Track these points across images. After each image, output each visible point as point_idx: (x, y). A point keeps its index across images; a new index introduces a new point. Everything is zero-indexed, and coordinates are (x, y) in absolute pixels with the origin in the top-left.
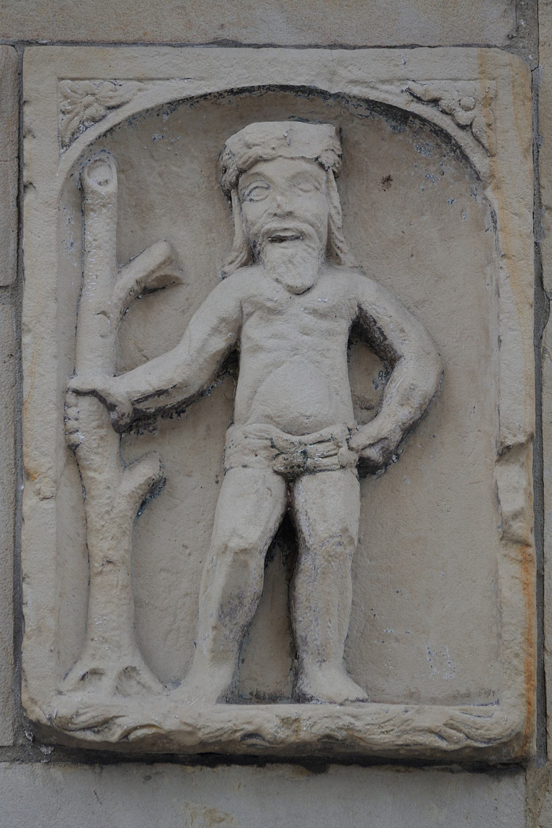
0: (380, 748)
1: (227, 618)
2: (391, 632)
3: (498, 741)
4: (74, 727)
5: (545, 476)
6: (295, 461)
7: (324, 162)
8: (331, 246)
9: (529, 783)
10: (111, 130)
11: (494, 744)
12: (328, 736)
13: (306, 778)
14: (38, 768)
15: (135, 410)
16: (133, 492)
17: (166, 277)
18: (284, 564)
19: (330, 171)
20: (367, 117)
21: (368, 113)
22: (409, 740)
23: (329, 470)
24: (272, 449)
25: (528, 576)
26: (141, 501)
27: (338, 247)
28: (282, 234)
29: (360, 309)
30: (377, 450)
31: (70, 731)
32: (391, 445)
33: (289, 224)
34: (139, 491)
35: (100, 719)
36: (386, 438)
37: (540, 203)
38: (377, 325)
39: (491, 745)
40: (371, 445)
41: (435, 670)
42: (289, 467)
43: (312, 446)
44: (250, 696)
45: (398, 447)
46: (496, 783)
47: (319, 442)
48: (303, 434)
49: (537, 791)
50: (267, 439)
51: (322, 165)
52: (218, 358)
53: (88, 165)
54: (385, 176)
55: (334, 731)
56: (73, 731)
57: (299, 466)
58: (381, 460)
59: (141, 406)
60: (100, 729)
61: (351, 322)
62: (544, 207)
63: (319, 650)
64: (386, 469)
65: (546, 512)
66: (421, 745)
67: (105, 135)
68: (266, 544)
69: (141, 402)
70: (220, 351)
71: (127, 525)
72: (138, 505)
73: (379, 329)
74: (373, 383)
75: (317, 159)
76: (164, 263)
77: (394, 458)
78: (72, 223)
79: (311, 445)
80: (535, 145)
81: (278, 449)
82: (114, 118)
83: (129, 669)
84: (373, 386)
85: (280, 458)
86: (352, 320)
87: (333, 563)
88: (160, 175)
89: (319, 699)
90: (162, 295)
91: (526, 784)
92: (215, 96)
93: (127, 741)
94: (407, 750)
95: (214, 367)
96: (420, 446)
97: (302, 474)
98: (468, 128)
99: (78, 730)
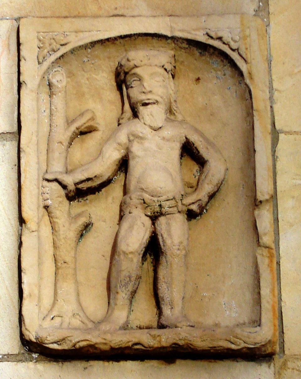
0: (201, 349)
1: (124, 288)
2: (206, 295)
3: (260, 344)
4: (48, 342)
5: (279, 217)
6: (156, 210)
7: (167, 68)
8: (171, 109)
9: (276, 366)
10: (62, 56)
11: (258, 346)
12: (175, 344)
13: (164, 366)
14: (31, 365)
15: (77, 189)
16: (76, 229)
17: (91, 127)
18: (152, 263)
19: (170, 73)
20: (187, 48)
21: (187, 46)
22: (216, 344)
23: (172, 214)
24: (144, 204)
25: (274, 299)
26: (80, 234)
27: (175, 110)
28: (147, 102)
29: (186, 138)
30: (196, 206)
31: (46, 344)
32: (203, 203)
33: (149, 96)
34: (79, 228)
35: (61, 338)
36: (200, 200)
37: (273, 88)
38: (195, 146)
39: (256, 346)
40: (193, 203)
41: (228, 312)
42: (152, 213)
43: (164, 202)
44: (136, 328)
45: (206, 205)
46: (259, 367)
47: (167, 200)
48: (159, 197)
49: (280, 370)
50: (141, 199)
51: (166, 70)
52: (117, 163)
53: (52, 73)
54: (197, 78)
55: (178, 341)
56: (47, 344)
57: (157, 212)
58: (198, 211)
59: (80, 186)
60: (61, 343)
61: (182, 145)
62: (274, 90)
63: (169, 303)
64: (201, 216)
65: (280, 234)
66: (221, 347)
67: (60, 58)
68: (142, 251)
69: (79, 184)
70: (118, 159)
71: (73, 244)
72: (79, 235)
73: (196, 148)
74: (194, 175)
75: (163, 66)
76: (90, 119)
77: (205, 211)
78: (45, 101)
79: (163, 202)
80: (269, 61)
81: (147, 204)
82: (63, 50)
83: (75, 314)
84: (194, 177)
85: (149, 208)
86: (182, 144)
87: (175, 259)
88: (88, 79)
89: (170, 326)
90: (89, 135)
91: (274, 367)
92: (113, 39)
93: (74, 348)
94: (214, 350)
95: (115, 167)
96: (217, 205)
97: (159, 216)
98: (236, 51)
99: (50, 344)
